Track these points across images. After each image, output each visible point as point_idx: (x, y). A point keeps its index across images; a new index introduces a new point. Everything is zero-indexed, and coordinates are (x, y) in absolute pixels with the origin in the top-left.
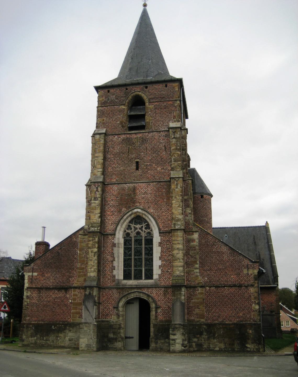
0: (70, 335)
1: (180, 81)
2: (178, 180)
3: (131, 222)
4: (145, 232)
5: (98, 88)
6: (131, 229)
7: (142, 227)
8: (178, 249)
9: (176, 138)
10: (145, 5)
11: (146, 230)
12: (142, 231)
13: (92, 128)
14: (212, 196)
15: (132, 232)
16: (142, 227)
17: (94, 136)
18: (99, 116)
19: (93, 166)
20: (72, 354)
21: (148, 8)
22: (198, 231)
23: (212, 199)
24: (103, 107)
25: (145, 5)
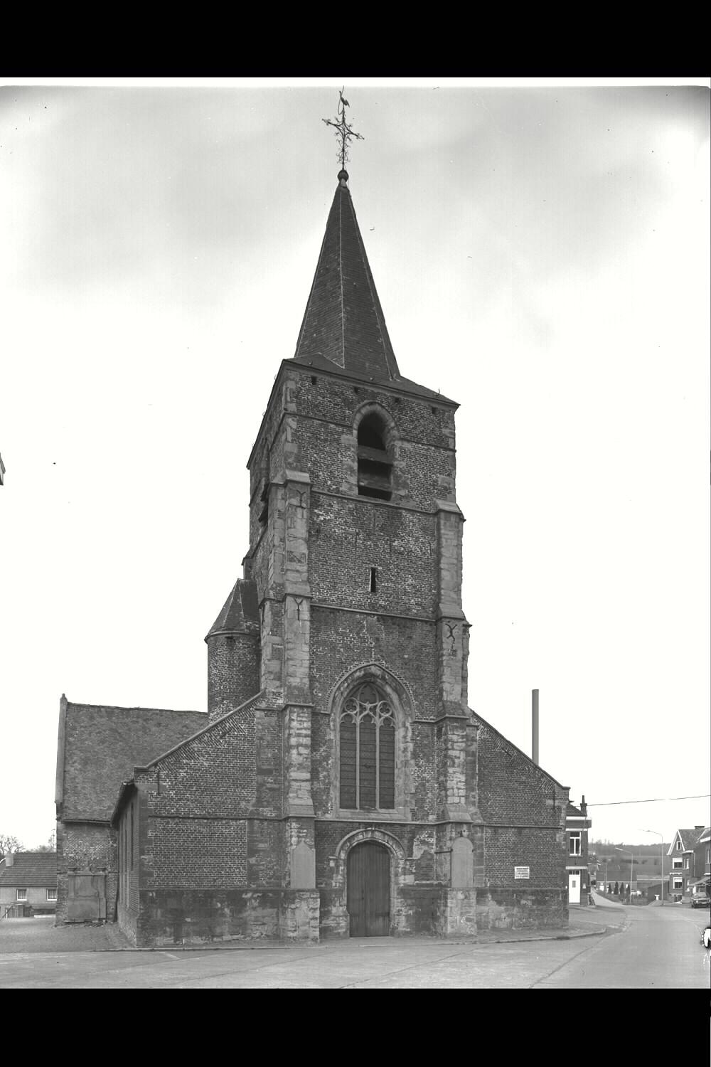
10: (343, 176)
21: (350, 184)
25: (343, 176)
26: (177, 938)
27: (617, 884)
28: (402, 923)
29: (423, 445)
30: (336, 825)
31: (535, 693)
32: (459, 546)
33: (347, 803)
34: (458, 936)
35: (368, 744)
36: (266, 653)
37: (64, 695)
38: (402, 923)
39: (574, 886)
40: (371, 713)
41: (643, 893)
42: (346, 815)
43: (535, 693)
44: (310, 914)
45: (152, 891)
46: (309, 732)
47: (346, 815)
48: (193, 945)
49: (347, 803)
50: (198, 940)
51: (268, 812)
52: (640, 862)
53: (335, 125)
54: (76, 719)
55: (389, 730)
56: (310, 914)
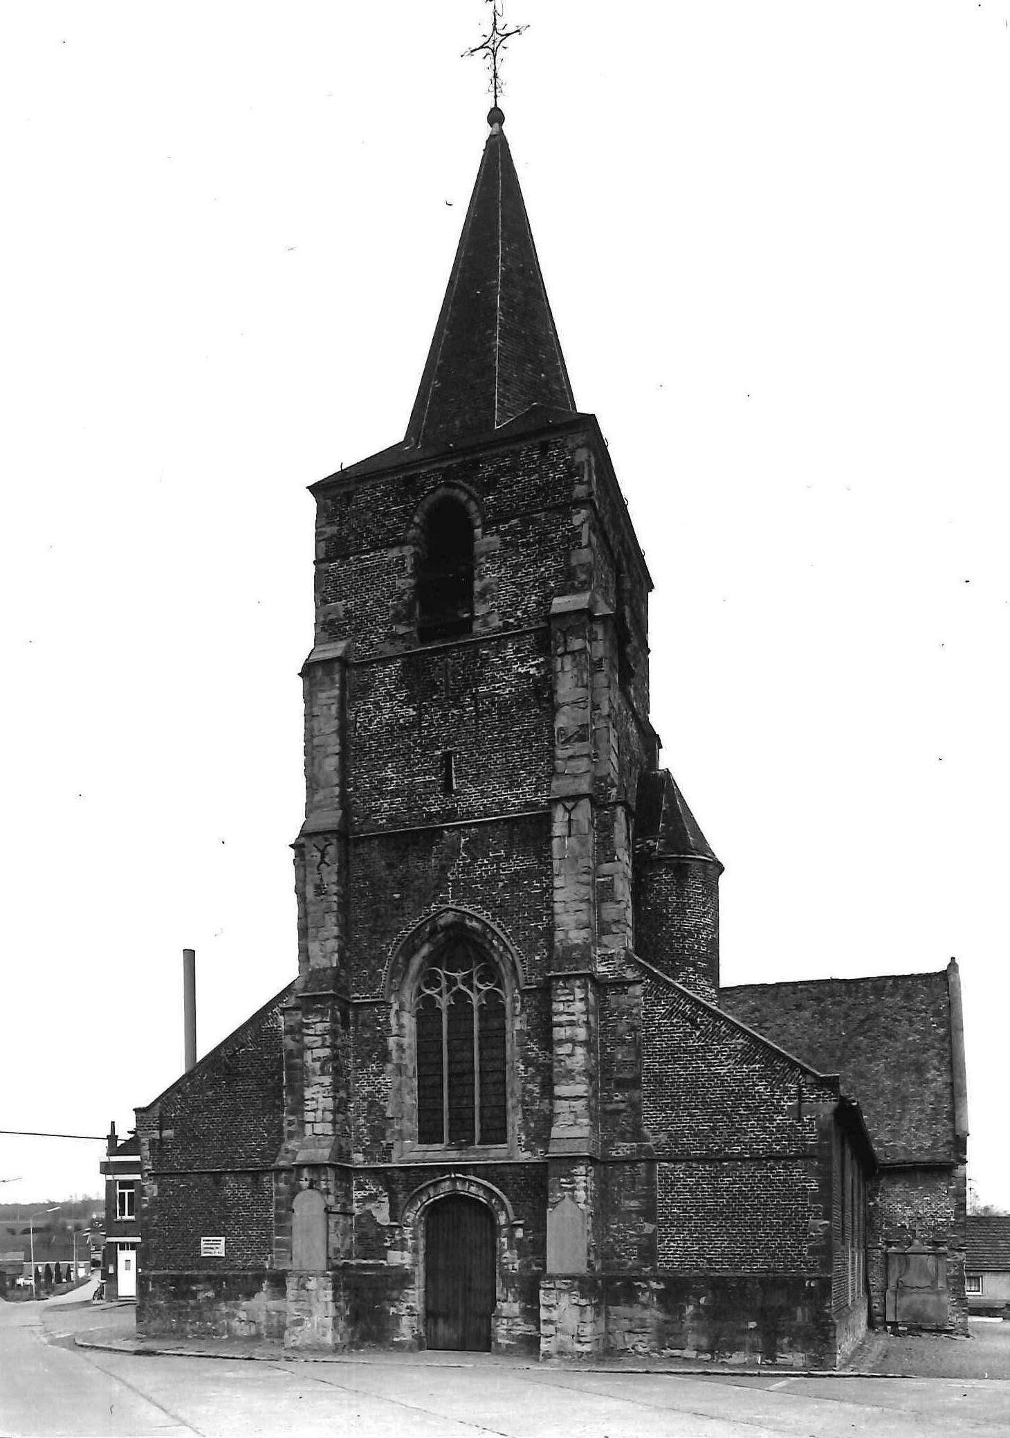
0: (263, 1302)
1: (592, 418)
2: (574, 808)
3: (433, 959)
4: (479, 990)
5: (315, 489)
6: (438, 984)
7: (470, 976)
8: (572, 1041)
9: (572, 653)
10: (496, 117)
11: (481, 986)
12: (471, 988)
13: (297, 634)
14: (721, 869)
15: (440, 994)
16: (470, 976)
17: (308, 671)
18: (322, 597)
19: (313, 785)
20: (818, 1167)
21: (507, 128)
22: (641, 982)
23: (721, 879)
24: (334, 550)
25: (496, 117)
26: (770, 1353)
27: (58, 1266)
28: (407, 1329)
29: (367, 552)
30: (503, 1169)
31: (190, 956)
32: (309, 716)
33: (428, 1135)
34: (400, 1346)
35: (461, 1037)
36: (623, 889)
37: (953, 959)
38: (407, 1329)
39: (127, 1268)
40: (464, 988)
41: (13, 1282)
42: (439, 1154)
43: (190, 955)
44: (555, 1315)
45: (811, 1279)
46: (556, 1019)
47: (439, 1154)
48: (790, 1367)
49: (428, 1135)
50: (797, 1359)
51: (623, 1149)
52: (18, 1232)
53: (495, 29)
54: (934, 995)
55: (494, 1010)
56: (555, 1315)
